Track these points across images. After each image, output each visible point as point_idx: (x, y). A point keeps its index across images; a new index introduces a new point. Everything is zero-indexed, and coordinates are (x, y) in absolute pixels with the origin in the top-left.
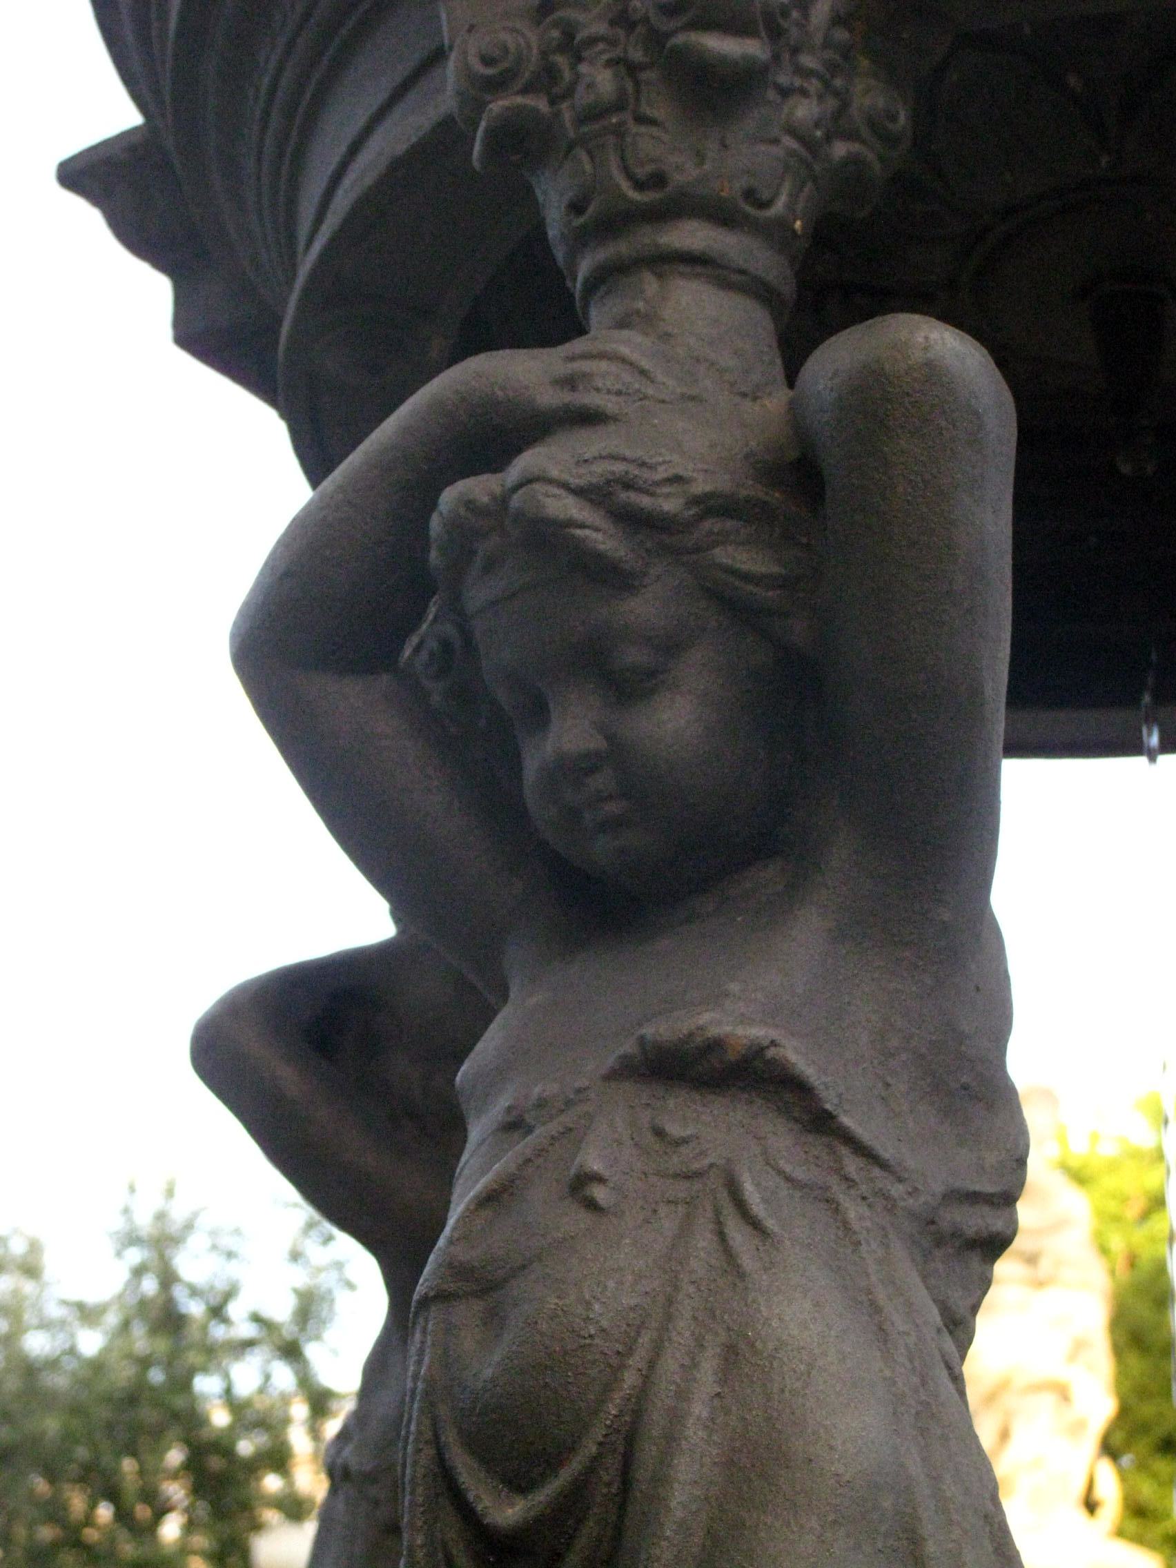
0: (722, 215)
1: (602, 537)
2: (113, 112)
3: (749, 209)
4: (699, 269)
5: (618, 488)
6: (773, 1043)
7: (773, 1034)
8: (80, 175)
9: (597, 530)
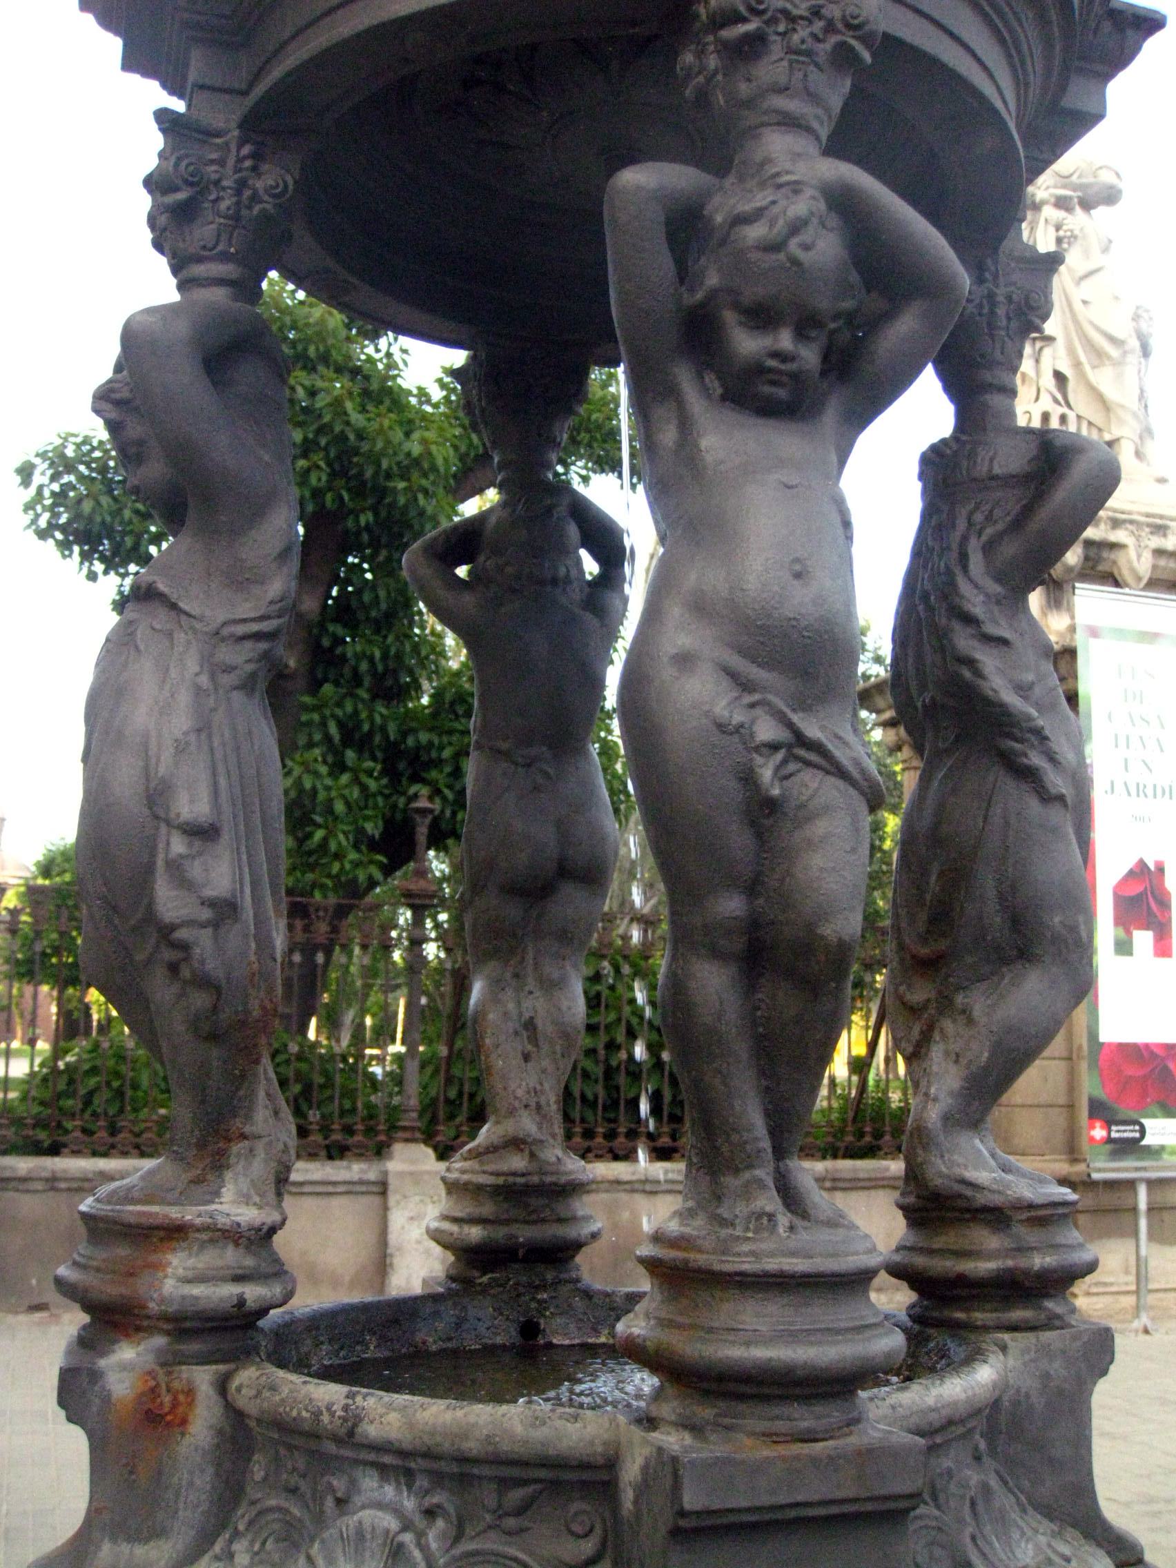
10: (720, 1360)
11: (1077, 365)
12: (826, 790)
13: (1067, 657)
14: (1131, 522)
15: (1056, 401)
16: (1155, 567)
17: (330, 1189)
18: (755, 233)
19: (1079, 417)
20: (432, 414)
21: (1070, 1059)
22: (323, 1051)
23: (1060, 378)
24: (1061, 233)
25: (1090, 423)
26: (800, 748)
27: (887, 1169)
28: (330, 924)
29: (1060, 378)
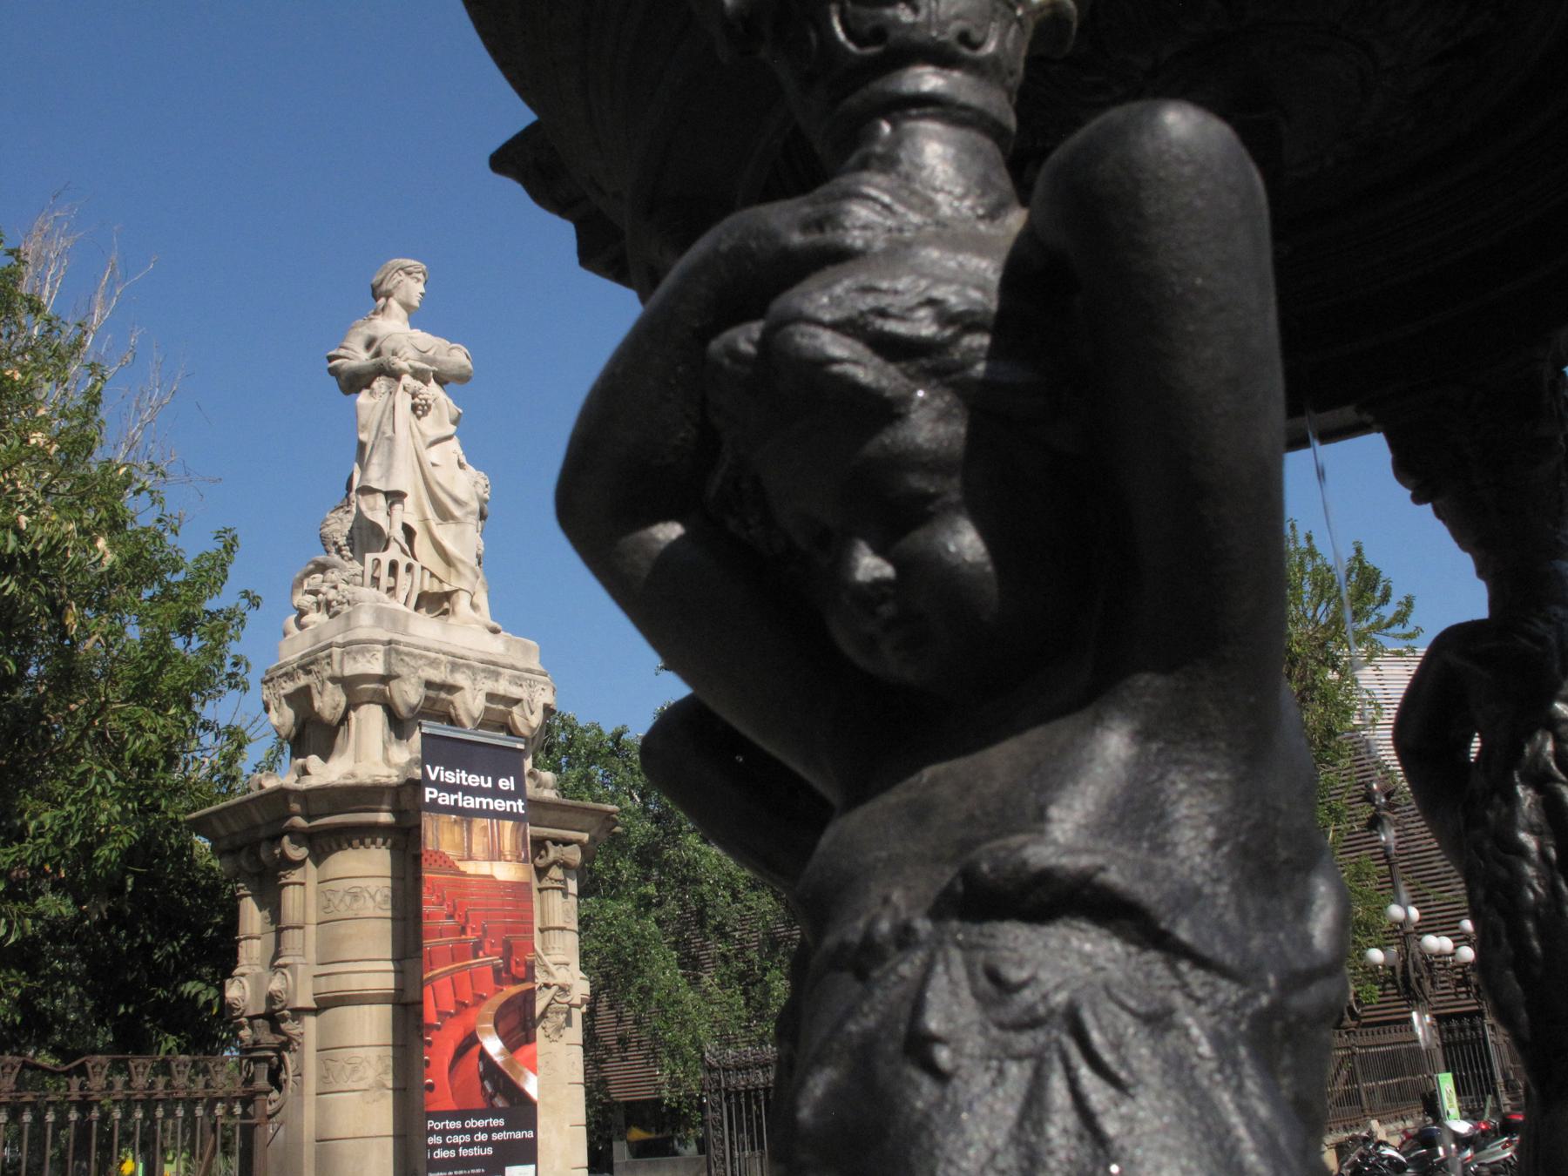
0: (942, 58)
1: (866, 370)
2: (517, 116)
3: (965, 51)
4: (930, 110)
5: (871, 318)
6: (1102, 869)
7: (1099, 860)
8: (503, 161)
9: (856, 362)
10: (960, 169)
11: (425, 520)
14: (469, 667)
15: (403, 551)
16: (487, 709)
19: (423, 568)
20: (1505, 1017)
22: (18, 1019)
23: (409, 532)
25: (432, 575)
29: (409, 532)
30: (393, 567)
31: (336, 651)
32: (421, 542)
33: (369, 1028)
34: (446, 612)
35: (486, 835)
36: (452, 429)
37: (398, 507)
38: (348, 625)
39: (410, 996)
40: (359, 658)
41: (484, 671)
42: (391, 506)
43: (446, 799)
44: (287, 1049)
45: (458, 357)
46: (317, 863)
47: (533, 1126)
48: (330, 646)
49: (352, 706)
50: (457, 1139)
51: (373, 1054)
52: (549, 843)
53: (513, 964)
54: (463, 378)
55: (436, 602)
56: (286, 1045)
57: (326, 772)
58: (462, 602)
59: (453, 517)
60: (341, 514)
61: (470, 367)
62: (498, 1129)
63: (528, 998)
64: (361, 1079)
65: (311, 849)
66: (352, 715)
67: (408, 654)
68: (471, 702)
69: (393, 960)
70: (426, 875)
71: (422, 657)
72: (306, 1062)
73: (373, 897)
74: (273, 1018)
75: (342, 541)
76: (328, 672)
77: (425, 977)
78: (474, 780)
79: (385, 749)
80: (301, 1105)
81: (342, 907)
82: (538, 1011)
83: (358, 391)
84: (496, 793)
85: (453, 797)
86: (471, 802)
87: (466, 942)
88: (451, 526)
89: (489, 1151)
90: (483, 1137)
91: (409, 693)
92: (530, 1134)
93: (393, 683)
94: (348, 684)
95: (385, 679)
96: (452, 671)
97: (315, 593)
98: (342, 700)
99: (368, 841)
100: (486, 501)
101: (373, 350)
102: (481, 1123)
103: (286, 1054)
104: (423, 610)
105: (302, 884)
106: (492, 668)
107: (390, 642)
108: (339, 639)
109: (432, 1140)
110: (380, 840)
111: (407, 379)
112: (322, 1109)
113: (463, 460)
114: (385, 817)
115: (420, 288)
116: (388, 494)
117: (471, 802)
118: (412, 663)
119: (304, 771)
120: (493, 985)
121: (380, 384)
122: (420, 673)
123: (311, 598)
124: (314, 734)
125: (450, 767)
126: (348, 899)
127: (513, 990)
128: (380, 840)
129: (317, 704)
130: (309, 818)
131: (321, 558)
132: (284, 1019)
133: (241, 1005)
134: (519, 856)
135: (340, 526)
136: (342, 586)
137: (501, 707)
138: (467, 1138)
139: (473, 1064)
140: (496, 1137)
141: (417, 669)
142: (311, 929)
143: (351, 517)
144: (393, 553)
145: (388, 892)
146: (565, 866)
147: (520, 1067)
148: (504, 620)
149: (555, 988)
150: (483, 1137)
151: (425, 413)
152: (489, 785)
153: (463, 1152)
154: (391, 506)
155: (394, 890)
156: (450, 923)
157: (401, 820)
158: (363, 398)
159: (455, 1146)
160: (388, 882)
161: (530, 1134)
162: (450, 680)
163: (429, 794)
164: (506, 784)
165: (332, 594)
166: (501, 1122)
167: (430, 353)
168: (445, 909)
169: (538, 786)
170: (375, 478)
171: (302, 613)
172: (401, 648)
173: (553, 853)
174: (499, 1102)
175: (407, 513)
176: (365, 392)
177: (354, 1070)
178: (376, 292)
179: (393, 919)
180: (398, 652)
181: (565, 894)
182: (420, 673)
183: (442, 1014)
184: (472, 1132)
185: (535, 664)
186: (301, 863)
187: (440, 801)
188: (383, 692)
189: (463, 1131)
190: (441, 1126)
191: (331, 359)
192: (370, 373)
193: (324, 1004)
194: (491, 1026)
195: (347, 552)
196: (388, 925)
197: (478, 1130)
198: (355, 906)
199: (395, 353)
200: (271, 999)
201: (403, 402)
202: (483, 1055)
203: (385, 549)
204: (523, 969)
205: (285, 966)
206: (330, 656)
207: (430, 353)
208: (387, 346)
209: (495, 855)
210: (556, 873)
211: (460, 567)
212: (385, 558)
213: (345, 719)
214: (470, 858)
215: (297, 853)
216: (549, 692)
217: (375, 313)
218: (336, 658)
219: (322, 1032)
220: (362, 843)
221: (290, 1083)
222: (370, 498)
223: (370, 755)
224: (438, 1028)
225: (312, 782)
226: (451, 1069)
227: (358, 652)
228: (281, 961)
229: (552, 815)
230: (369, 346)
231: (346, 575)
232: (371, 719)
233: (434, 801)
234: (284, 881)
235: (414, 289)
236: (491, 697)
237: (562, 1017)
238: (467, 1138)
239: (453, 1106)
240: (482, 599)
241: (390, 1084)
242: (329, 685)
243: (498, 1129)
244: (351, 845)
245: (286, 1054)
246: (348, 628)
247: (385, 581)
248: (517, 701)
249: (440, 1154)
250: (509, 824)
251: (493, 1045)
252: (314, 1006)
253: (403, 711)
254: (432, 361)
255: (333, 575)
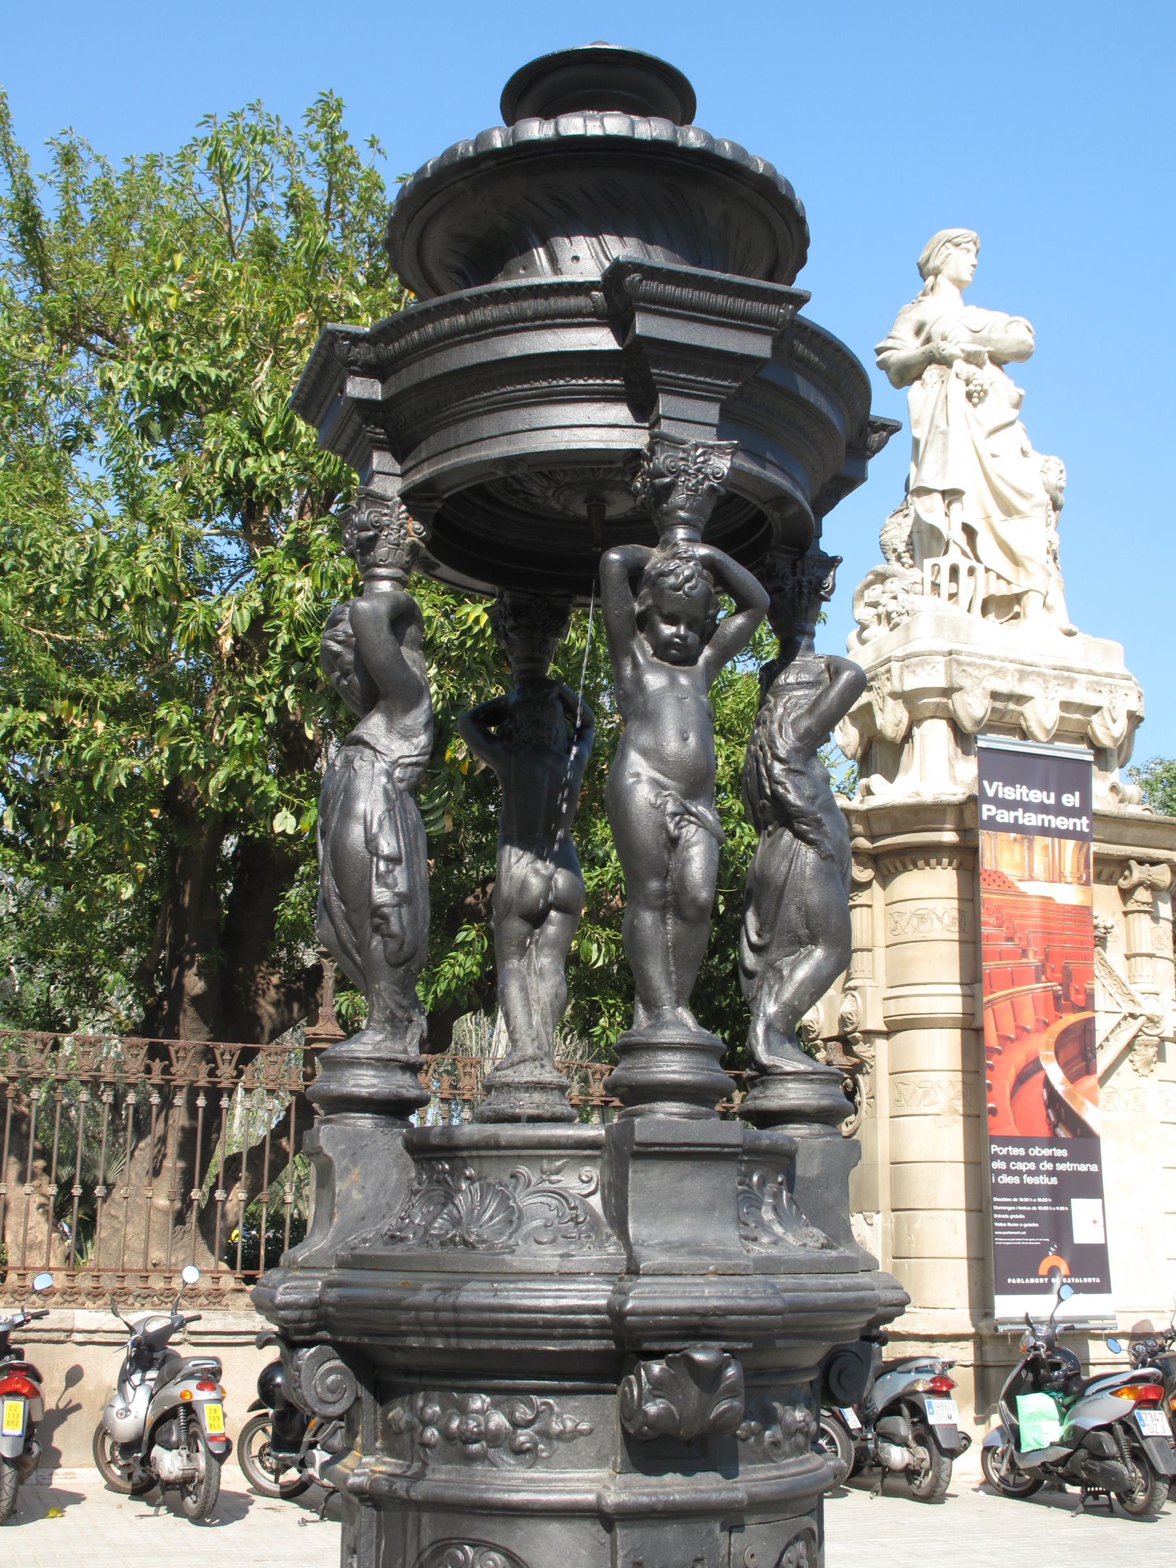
12: (796, 1131)
13: (972, 806)
14: (1039, 674)
15: (964, 553)
16: (1062, 719)
17: (230, 1339)
18: (671, 580)
19: (987, 570)
21: (980, 1211)
23: (969, 532)
24: (971, 387)
25: (999, 577)
26: (767, 1119)
27: (759, 1138)
28: (236, 1068)
30: (954, 571)
31: (895, 666)
32: (984, 541)
33: (941, 1051)
34: (1017, 616)
35: (1046, 856)
36: (1015, 413)
37: (955, 506)
38: (908, 636)
39: (976, 1025)
40: (919, 670)
41: (1056, 678)
42: (948, 506)
43: (1005, 816)
44: (861, 1072)
45: (1012, 331)
46: (884, 886)
47: (1095, 1157)
48: (889, 660)
49: (914, 722)
50: (1021, 1166)
51: (945, 1078)
52: (1133, 863)
53: (1072, 991)
54: (1023, 356)
55: (1003, 606)
56: (858, 1068)
57: (886, 792)
58: (1032, 604)
59: (1018, 512)
60: (899, 518)
61: (1031, 341)
62: (1062, 1160)
63: (1087, 1027)
64: (932, 1103)
65: (877, 869)
66: (916, 731)
67: (969, 664)
68: (1042, 715)
69: (961, 984)
70: (984, 896)
71: (986, 666)
72: (877, 1086)
73: (940, 919)
74: (845, 1041)
75: (901, 548)
76: (888, 688)
77: (985, 999)
78: (1037, 796)
79: (951, 765)
80: (875, 1127)
81: (909, 929)
82: (1098, 1042)
83: (910, 383)
84: (1060, 810)
85: (1013, 814)
86: (1033, 820)
87: (1027, 965)
88: (1015, 521)
89: (1054, 1181)
90: (1048, 1166)
91: (973, 706)
92: (1094, 1168)
93: (956, 696)
94: (908, 698)
95: (947, 692)
96: (1020, 680)
97: (875, 605)
98: (904, 717)
99: (933, 861)
100: (1061, 489)
101: (923, 336)
102: (1047, 1152)
103: (859, 1077)
104: (991, 616)
105: (870, 906)
106: (1066, 674)
107: (950, 653)
108: (899, 653)
109: (997, 1165)
110: (945, 861)
111: (959, 365)
112: (895, 1133)
113: (1028, 447)
114: (949, 837)
115: (972, 259)
116: (944, 493)
117: (1033, 820)
118: (976, 673)
119: (868, 792)
120: (1053, 1012)
121: (932, 373)
122: (985, 684)
123: (873, 611)
124: (880, 755)
125: (1009, 782)
126: (915, 921)
127: (1071, 1018)
128: (945, 861)
129: (879, 721)
130: (872, 838)
131: (881, 567)
132: (857, 1042)
133: (816, 1027)
134: (1080, 878)
135: (898, 532)
136: (902, 596)
137: (1078, 716)
138: (1032, 1166)
139: (1035, 1093)
140: (1061, 1167)
141: (980, 680)
142: (880, 952)
143: (910, 521)
144: (954, 556)
145: (955, 914)
146: (1153, 888)
147: (1080, 1097)
148: (1083, 620)
149: (1142, 1020)
150: (1048, 1166)
151: (981, 399)
152: (1052, 801)
153: (1028, 1180)
154: (948, 506)
155: (961, 911)
156: (1009, 945)
157: (958, 841)
158: (915, 391)
159: (1019, 1173)
160: (955, 903)
161: (1094, 1168)
162: (1019, 690)
163: (987, 811)
164: (1071, 800)
165: (892, 606)
166: (1063, 1153)
167: (984, 334)
168: (1004, 932)
169: (1121, 801)
170: (930, 475)
171: (864, 627)
172: (962, 658)
173: (1138, 873)
174: (1062, 1133)
175: (962, 512)
176: (917, 383)
177: (925, 1094)
178: (924, 271)
179: (961, 942)
180: (958, 663)
181: (1156, 918)
182: (985, 684)
183: (1004, 1039)
184: (1037, 1160)
185: (1118, 667)
186: (867, 885)
187: (998, 819)
188: (946, 706)
189: (1027, 1158)
190: (1004, 1151)
191: (879, 351)
192: (920, 363)
193: (894, 1028)
194: (1052, 1053)
195: (906, 559)
196: (956, 947)
197: (1043, 1158)
198: (922, 928)
199: (944, 339)
200: (843, 1021)
201: (957, 389)
202: (1047, 1084)
203: (946, 552)
204: (1082, 997)
205: (855, 989)
206: (889, 671)
207: (984, 334)
208: (936, 330)
209: (1055, 876)
210: (1143, 895)
211: (1028, 564)
212: (945, 562)
213: (908, 737)
214: (1032, 878)
215: (862, 874)
216: (1134, 696)
217: (924, 295)
218: (895, 672)
219: (893, 1055)
220: (927, 864)
221: (864, 1105)
222: (925, 499)
223: (935, 771)
224: (999, 1052)
225: (873, 802)
226: (1012, 1096)
227: (917, 665)
228: (851, 984)
229: (1132, 833)
230: (918, 331)
231: (905, 584)
232: (934, 736)
233: (992, 819)
234: (851, 903)
235: (960, 262)
236: (1066, 706)
237: (1152, 1051)
238: (1032, 1166)
239: (1015, 1132)
240: (1057, 599)
241: (960, 1109)
242: (890, 701)
243: (1062, 1160)
244: (916, 866)
245: (859, 1077)
246: (908, 640)
247: (947, 587)
248: (1097, 709)
249: (1005, 1179)
250: (1070, 844)
251: (1055, 1074)
252: (885, 1029)
253: (968, 725)
254: (985, 342)
255: (892, 585)
